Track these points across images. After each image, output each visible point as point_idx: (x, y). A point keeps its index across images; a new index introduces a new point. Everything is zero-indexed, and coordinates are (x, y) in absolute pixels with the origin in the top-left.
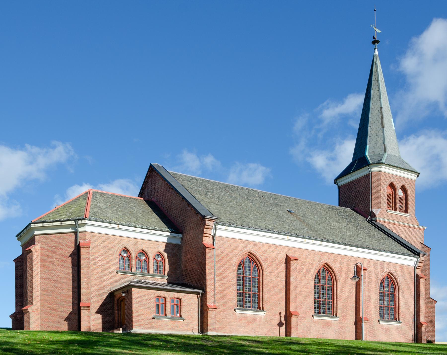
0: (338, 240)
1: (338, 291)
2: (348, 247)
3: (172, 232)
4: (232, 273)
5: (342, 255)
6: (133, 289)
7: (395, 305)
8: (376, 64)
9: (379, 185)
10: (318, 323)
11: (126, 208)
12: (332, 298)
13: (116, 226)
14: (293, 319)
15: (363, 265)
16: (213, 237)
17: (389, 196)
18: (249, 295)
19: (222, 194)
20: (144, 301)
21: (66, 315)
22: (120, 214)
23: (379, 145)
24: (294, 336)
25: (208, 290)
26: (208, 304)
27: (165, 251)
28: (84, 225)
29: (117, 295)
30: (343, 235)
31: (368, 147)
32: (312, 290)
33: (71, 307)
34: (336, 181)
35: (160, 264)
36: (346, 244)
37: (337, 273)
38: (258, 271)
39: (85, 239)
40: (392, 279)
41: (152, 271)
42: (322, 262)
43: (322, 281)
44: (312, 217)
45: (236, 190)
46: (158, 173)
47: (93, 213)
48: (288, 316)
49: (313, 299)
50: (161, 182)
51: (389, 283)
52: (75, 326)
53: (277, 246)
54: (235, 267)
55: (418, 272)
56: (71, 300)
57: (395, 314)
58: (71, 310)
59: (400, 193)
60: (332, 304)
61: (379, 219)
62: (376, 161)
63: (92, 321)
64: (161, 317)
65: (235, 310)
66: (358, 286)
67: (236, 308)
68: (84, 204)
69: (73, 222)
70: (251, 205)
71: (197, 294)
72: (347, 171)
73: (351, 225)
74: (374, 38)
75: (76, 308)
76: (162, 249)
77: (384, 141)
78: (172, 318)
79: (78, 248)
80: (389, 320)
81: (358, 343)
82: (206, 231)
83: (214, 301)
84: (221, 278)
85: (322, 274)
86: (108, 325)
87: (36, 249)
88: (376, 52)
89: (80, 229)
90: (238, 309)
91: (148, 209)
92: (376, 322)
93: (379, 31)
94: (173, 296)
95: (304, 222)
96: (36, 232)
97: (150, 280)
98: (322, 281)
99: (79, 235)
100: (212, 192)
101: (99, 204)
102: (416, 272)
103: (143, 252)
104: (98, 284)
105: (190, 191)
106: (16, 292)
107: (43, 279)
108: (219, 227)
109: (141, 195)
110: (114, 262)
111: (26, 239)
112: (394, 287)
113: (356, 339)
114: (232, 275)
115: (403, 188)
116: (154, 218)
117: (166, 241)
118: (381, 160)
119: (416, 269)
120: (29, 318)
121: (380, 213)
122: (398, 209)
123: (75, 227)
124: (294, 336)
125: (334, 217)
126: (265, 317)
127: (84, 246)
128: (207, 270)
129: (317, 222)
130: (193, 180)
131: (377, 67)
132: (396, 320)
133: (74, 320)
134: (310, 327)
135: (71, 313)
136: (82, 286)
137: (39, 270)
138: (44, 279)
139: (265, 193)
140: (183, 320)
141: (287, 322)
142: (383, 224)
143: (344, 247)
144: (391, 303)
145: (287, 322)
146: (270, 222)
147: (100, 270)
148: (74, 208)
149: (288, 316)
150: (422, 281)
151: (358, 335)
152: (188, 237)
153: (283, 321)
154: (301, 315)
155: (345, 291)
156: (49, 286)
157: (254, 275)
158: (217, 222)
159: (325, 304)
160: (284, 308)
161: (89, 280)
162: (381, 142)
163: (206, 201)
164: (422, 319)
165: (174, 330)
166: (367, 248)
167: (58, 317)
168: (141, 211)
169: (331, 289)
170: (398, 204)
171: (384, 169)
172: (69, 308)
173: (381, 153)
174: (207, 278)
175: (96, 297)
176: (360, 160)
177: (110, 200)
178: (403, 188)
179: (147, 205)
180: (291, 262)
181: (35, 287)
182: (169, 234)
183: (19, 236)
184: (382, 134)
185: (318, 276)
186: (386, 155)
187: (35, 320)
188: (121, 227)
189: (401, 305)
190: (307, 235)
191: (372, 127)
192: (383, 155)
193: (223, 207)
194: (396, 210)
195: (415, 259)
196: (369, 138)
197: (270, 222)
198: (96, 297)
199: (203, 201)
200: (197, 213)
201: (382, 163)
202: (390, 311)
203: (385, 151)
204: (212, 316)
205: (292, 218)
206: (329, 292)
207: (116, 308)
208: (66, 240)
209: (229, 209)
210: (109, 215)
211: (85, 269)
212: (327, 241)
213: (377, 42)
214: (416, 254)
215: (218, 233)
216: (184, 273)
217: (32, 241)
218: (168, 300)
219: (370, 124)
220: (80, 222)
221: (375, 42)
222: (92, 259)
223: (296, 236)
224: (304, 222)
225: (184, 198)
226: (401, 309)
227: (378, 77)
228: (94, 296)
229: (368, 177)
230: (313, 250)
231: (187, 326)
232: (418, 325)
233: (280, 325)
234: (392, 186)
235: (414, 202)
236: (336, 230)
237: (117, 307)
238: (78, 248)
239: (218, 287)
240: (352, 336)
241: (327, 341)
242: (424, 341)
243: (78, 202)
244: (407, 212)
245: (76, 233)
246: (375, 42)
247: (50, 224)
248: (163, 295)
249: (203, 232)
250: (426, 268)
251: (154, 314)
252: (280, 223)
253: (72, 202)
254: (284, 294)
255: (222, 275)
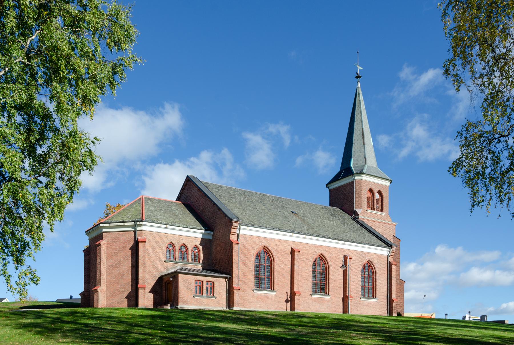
0: (330, 236)
1: (330, 276)
2: (337, 241)
3: (206, 230)
4: (251, 262)
5: (333, 247)
6: (179, 275)
7: (373, 286)
8: (359, 94)
9: (361, 190)
10: (315, 300)
11: (170, 211)
12: (325, 281)
13: (165, 226)
14: (297, 297)
15: (349, 255)
16: (238, 235)
17: (368, 199)
18: (264, 279)
19: (242, 199)
20: (187, 284)
21: (126, 294)
22: (167, 216)
23: (361, 158)
24: (297, 310)
25: (234, 275)
26: (234, 285)
27: (200, 244)
28: (141, 225)
29: (165, 279)
30: (334, 231)
31: (352, 159)
32: (310, 274)
33: (130, 288)
34: (327, 186)
35: (196, 255)
36: (336, 239)
37: (329, 261)
38: (270, 260)
39: (142, 236)
40: (370, 266)
41: (190, 260)
42: (318, 253)
43: (318, 267)
44: (310, 217)
45: (252, 195)
46: (192, 181)
47: (148, 216)
48: (293, 295)
49: (311, 281)
50: (196, 190)
51: (368, 269)
52: (133, 303)
53: (285, 241)
54: (253, 257)
55: (390, 260)
56: (130, 283)
57: (373, 293)
58: (130, 290)
59: (377, 196)
60: (325, 285)
61: (360, 217)
62: (359, 171)
63: (146, 299)
64: (199, 296)
65: (253, 291)
66: (345, 272)
67: (254, 288)
68: (140, 208)
69: (133, 223)
70: (264, 207)
71: (226, 278)
72: (336, 178)
73: (339, 222)
74: (357, 74)
75: (134, 288)
76: (198, 243)
77: (365, 155)
78: (207, 297)
79: (136, 243)
80: (368, 297)
81: (345, 316)
82: (233, 230)
83: (238, 283)
84: (243, 266)
85: (318, 262)
86: (158, 303)
87: (104, 243)
88: (359, 85)
89: (138, 229)
90: (256, 290)
91: (187, 211)
92: (359, 299)
93: (361, 69)
94: (208, 280)
95: (304, 221)
96: (104, 230)
97: (189, 267)
98: (318, 267)
99: (137, 232)
100: (234, 198)
101: (150, 208)
102: (389, 260)
103: (184, 245)
104: (152, 270)
105: (219, 198)
106: (85, 276)
107: (108, 266)
108: (242, 227)
109: (178, 199)
110: (163, 254)
111: (94, 234)
112: (372, 272)
113: (343, 312)
114: (251, 264)
115: (380, 192)
116: (191, 219)
117: (201, 237)
118: (362, 170)
119: (389, 258)
120: (98, 296)
121: (362, 212)
122: (375, 209)
123: (134, 226)
124: (297, 310)
125: (326, 216)
126: (276, 296)
127: (142, 242)
128: (233, 260)
129: (313, 220)
130: (220, 188)
131: (359, 96)
132: (374, 297)
133: (133, 299)
134: (310, 304)
135: (130, 293)
136: (139, 272)
137: (106, 259)
138: (110, 266)
139: (273, 197)
140: (215, 298)
141: (291, 299)
142: (364, 221)
143: (334, 241)
144: (370, 284)
145: (291, 299)
146: (279, 222)
147: (152, 260)
148: (132, 211)
149: (293, 295)
150: (394, 267)
151: (345, 310)
152: (218, 234)
153: (289, 299)
154: (302, 294)
155: (335, 276)
156: (113, 271)
157: (268, 264)
158: (241, 223)
159: (320, 285)
160: (290, 289)
161: (145, 267)
162: (363, 156)
163: (231, 206)
164: (394, 297)
165: (208, 306)
166: (352, 242)
167: (120, 295)
168: (181, 213)
169: (325, 274)
170: (375, 205)
171: (364, 177)
172: (128, 289)
173: (363, 164)
174: (233, 266)
175: (149, 281)
176: (346, 170)
177: (158, 204)
178: (380, 192)
179: (185, 208)
180: (295, 253)
181: (102, 273)
182: (203, 231)
183: (88, 232)
184: (363, 150)
185: (315, 264)
186: (366, 166)
187: (103, 299)
188: (168, 226)
189: (377, 286)
190: (307, 232)
191: (356, 144)
192: (364, 166)
193: (244, 210)
194: (374, 209)
195: (388, 250)
196: (353, 152)
197: (279, 222)
198: (149, 281)
199: (229, 206)
200: (226, 216)
201: (363, 173)
202: (369, 290)
203: (366, 163)
204: (237, 295)
205: (295, 218)
206: (323, 276)
207: (164, 289)
208: (127, 236)
209: (248, 212)
210: (159, 217)
211: (142, 259)
212: (322, 236)
213: (360, 77)
214: (389, 246)
215: (242, 232)
216: (214, 261)
217: (100, 237)
218: (205, 283)
219: (354, 142)
220: (138, 223)
221: (358, 77)
222: (147, 251)
223: (299, 233)
224: (304, 221)
225: (215, 204)
226: (378, 289)
227: (360, 105)
228: (148, 279)
229: (352, 184)
230: (311, 244)
231: (217, 303)
232: (390, 301)
233: (287, 301)
234: (371, 190)
235: (388, 203)
236: (328, 227)
237: (166, 289)
238: (136, 243)
239: (241, 273)
240: (340, 311)
241: (324, 315)
242: (395, 314)
243: (134, 206)
244: (382, 211)
245: (135, 232)
246: (358, 77)
247: (115, 224)
248: (201, 279)
249: (230, 231)
250: (397, 257)
251: (194, 294)
252: (286, 222)
253: (129, 206)
254: (290, 278)
255: (244, 264)
